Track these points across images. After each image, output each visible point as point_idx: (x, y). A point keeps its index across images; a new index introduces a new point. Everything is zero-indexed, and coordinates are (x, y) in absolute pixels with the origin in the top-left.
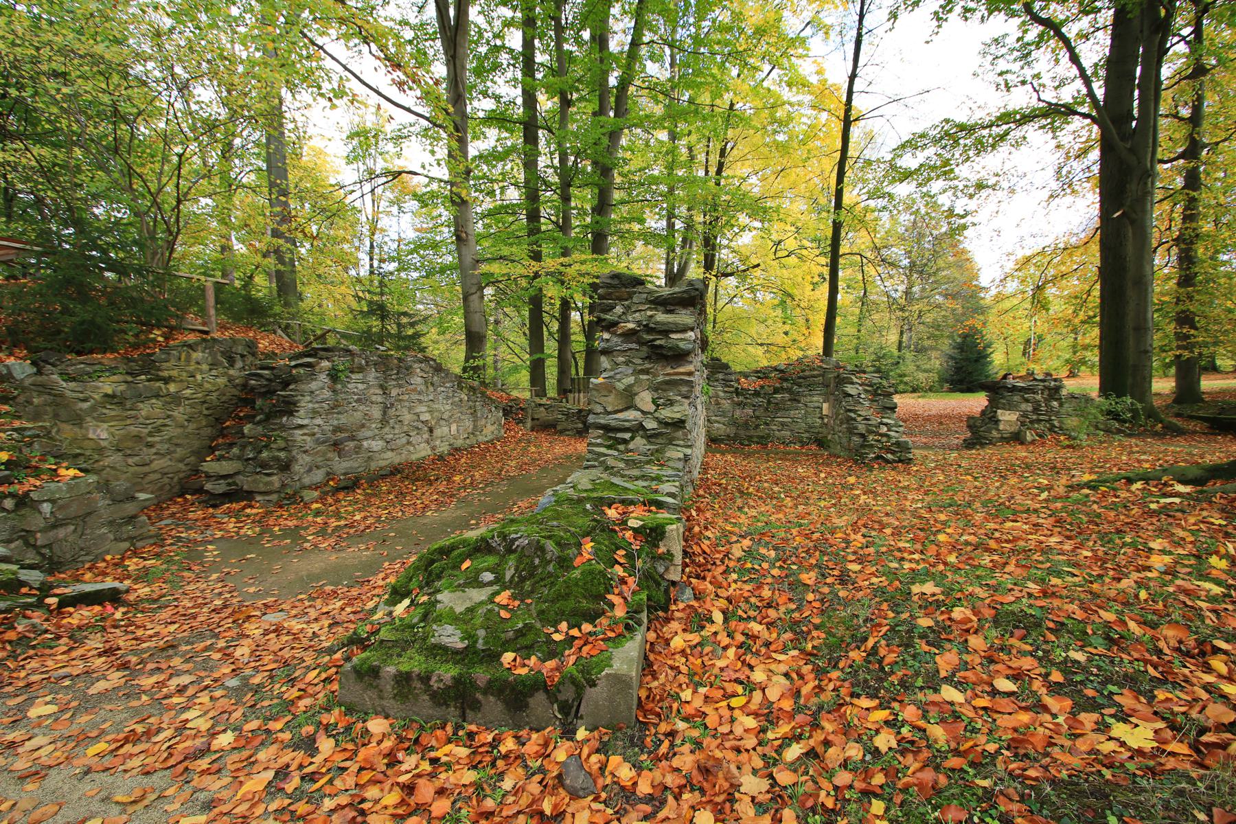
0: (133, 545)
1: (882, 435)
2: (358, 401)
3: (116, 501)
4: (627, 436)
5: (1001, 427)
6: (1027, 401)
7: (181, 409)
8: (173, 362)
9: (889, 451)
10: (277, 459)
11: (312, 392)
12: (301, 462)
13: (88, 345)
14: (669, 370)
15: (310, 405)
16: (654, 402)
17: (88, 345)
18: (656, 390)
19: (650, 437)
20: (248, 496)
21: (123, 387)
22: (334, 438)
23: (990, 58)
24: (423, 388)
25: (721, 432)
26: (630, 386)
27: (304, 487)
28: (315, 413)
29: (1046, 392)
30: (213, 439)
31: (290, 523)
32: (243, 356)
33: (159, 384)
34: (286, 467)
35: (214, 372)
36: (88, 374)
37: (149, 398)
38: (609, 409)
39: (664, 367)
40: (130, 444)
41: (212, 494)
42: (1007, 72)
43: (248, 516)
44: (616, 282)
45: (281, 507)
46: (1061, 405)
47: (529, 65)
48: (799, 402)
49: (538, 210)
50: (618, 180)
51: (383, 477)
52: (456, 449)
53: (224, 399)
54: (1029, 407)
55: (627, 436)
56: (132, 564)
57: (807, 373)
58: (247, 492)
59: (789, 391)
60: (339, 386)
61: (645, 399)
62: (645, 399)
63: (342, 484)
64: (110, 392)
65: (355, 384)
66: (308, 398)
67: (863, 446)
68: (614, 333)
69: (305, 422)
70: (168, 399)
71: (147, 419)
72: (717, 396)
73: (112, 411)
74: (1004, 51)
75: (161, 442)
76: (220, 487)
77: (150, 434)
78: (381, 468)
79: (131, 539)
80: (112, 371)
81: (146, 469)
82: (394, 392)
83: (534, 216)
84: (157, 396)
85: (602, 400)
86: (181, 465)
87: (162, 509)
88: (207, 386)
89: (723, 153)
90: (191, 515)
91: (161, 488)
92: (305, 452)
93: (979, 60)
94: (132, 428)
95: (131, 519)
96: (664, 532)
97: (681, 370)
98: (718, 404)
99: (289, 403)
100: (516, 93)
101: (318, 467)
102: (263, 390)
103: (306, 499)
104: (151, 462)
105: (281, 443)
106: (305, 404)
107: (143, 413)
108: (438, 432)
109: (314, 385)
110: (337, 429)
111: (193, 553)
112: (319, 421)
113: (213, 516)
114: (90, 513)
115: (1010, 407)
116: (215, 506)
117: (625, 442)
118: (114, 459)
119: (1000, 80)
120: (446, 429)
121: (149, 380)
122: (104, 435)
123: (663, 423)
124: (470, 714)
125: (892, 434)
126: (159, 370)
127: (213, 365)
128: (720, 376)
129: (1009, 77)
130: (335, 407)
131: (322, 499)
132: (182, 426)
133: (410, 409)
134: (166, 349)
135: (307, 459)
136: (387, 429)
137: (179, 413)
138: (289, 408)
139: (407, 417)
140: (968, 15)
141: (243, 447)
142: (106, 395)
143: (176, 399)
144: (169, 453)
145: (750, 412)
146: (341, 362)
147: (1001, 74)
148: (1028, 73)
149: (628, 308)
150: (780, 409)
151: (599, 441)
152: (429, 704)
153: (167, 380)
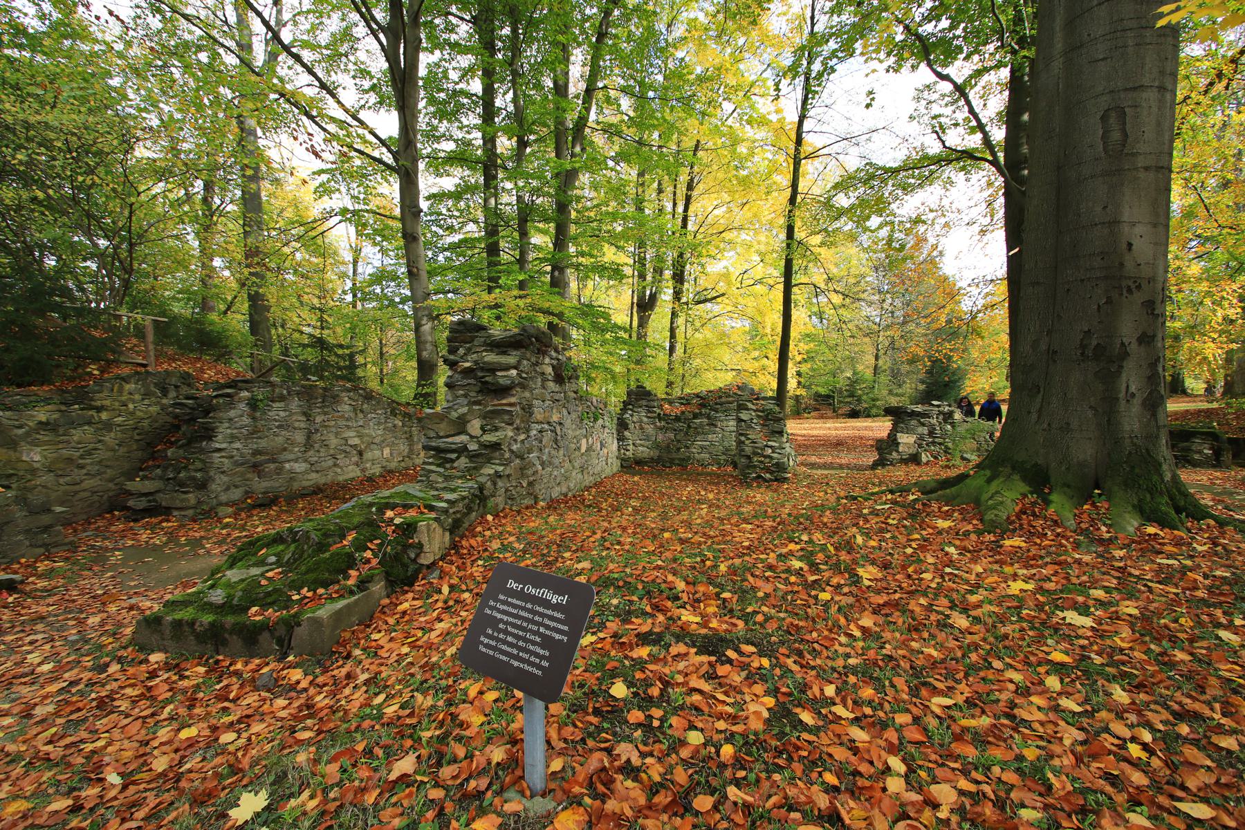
0: (48, 550)
1: (765, 457)
2: (278, 427)
3: (31, 513)
4: (454, 456)
5: (901, 449)
6: (923, 425)
7: (112, 435)
8: (106, 393)
9: (768, 470)
10: (194, 478)
11: (231, 419)
12: (218, 481)
13: (27, 379)
14: (496, 402)
15: (229, 431)
16: (482, 428)
17: (27, 379)
18: (484, 418)
19: (473, 456)
20: (166, 512)
22: (253, 460)
23: (924, 103)
24: (352, 415)
25: (645, 455)
26: (464, 415)
27: (221, 504)
28: (233, 439)
29: (941, 417)
30: (143, 461)
31: (197, 535)
32: (176, 387)
33: (93, 413)
34: (202, 486)
35: (146, 402)
36: (24, 404)
37: (81, 425)
38: (441, 434)
39: (492, 400)
40: (62, 465)
41: (135, 511)
42: (940, 116)
43: (163, 529)
44: (462, 328)
45: (195, 521)
47: (489, 113)
48: (716, 426)
49: (497, 243)
50: (573, 214)
51: (303, 496)
52: (390, 472)
53: (156, 425)
54: (925, 430)
56: (42, 567)
57: (723, 400)
59: (709, 417)
60: (258, 414)
61: (475, 426)
62: (475, 426)
63: (259, 502)
64: (44, 419)
65: (277, 411)
66: (227, 425)
67: (748, 467)
69: (223, 446)
70: (99, 426)
71: (79, 443)
72: (641, 421)
73: (44, 436)
74: (935, 96)
75: (91, 464)
76: (141, 504)
77: (82, 457)
78: (304, 488)
79: (45, 545)
80: (47, 401)
81: (77, 488)
82: (319, 419)
83: (493, 250)
84: (89, 423)
85: (435, 427)
86: (111, 485)
87: (90, 523)
88: (139, 414)
89: (690, 187)
90: (113, 528)
91: (91, 505)
92: (223, 472)
93: (914, 105)
94: (64, 451)
95: (46, 529)
96: (416, 528)
97: (504, 401)
98: (642, 428)
99: (207, 429)
100: (477, 137)
101: (236, 487)
103: (220, 514)
104: (82, 481)
105: (198, 465)
106: (223, 430)
107: (75, 438)
108: (368, 455)
109: (232, 413)
110: (256, 452)
111: (100, 558)
112: (237, 445)
113: (131, 529)
114: (7, 523)
115: (908, 431)
116: (135, 521)
117: (452, 461)
118: (46, 478)
120: (377, 453)
121: (82, 409)
122: (37, 458)
123: (483, 446)
124: (221, 649)
125: (775, 455)
127: (147, 395)
128: (644, 402)
130: (254, 432)
131: (235, 515)
132: (113, 450)
133: (337, 434)
134: (100, 381)
135: (225, 479)
136: (311, 453)
137: (110, 438)
138: (208, 434)
139: (334, 442)
141: (165, 469)
142: (41, 423)
143: (108, 426)
144: (99, 473)
145: (672, 436)
146: (260, 393)
149: (469, 350)
150: (698, 433)
152: (194, 642)
153: (99, 409)
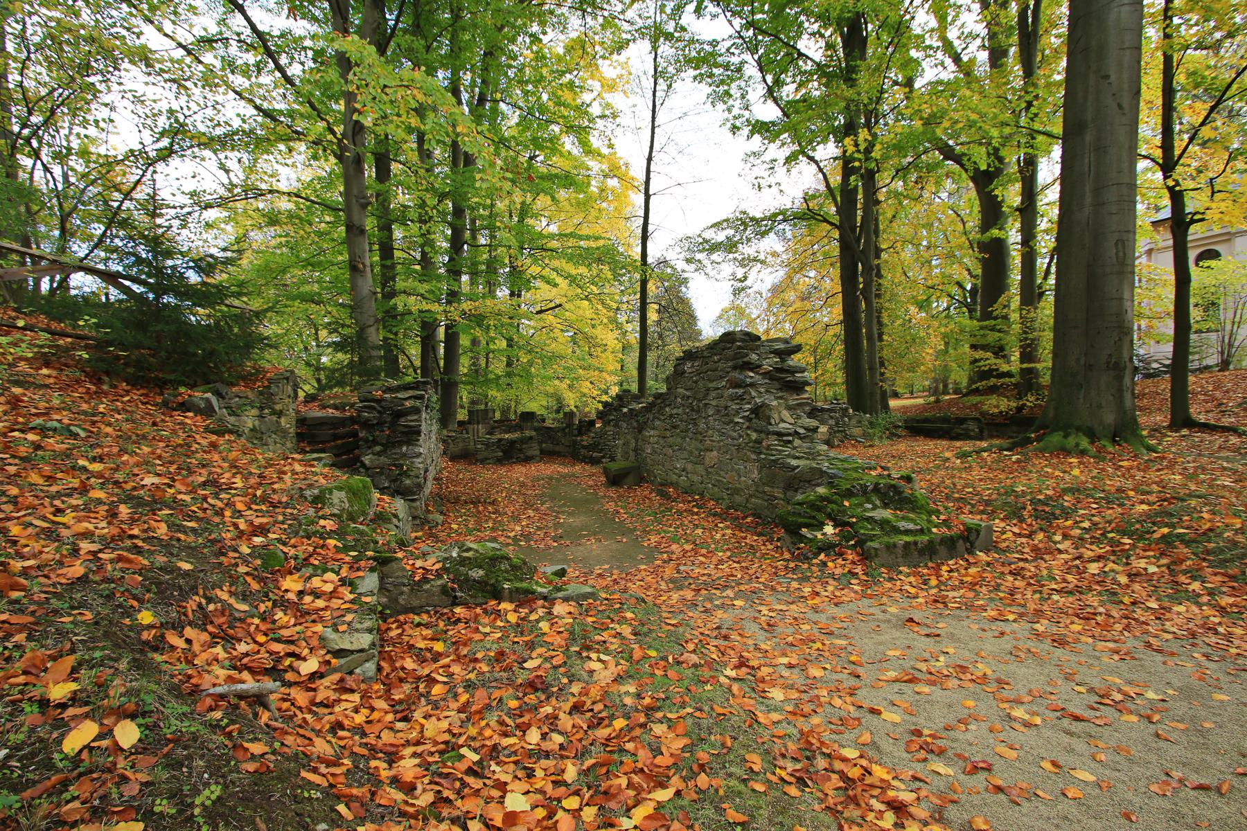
68: (757, 373)
117: (790, 442)
119: (755, 182)
148: (772, 180)
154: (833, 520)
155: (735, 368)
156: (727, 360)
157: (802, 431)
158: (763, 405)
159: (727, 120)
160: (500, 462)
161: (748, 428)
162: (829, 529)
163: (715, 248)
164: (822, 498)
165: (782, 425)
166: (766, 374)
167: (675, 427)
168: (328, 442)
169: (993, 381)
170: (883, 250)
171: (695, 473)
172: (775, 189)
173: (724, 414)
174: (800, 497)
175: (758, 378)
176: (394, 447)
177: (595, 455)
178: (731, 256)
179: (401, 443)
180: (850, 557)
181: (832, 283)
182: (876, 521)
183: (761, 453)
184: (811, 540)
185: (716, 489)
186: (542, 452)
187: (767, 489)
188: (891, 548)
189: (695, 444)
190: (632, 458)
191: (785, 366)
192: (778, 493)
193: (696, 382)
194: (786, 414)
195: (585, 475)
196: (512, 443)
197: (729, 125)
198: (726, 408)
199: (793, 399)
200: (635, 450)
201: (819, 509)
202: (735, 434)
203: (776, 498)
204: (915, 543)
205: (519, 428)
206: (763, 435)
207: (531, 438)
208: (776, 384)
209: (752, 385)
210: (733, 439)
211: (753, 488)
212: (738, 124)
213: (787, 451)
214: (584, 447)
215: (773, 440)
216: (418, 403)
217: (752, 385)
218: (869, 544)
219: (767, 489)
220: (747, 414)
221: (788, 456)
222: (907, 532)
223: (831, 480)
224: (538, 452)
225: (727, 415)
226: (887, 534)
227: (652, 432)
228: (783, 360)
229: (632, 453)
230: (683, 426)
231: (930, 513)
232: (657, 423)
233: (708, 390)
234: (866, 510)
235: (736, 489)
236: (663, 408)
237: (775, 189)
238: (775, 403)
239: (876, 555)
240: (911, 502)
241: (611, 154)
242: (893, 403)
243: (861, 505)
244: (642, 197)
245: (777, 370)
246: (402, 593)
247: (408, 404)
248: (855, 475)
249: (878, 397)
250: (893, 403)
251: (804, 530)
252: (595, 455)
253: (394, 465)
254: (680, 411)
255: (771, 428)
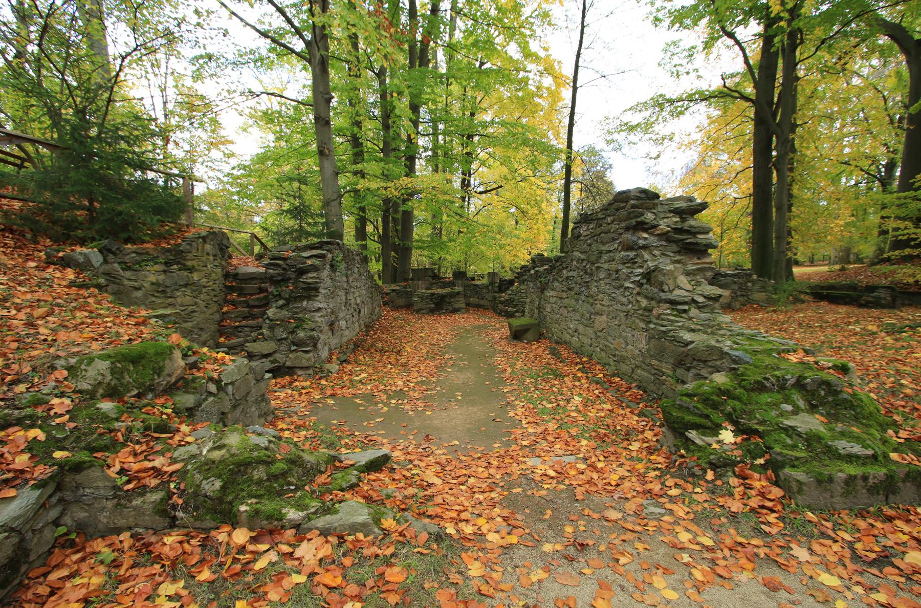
4: (686, 307)
21: (162, 277)
23: (669, 54)
36: (139, 263)
39: (691, 258)
44: (643, 196)
46: (753, 285)
55: (686, 307)
58: (288, 368)
64: (154, 281)
68: (652, 234)
93: (662, 55)
102: (280, 278)
117: (685, 311)
119: (674, 70)
126: (186, 260)
129: (679, 68)
140: (658, 23)
147: (675, 66)
148: (690, 67)
151: (668, 311)
153: (191, 270)
154: (735, 423)
155: (627, 229)
156: (621, 221)
157: (701, 299)
158: (656, 269)
159: (651, 13)
160: (432, 312)
161: (638, 294)
162: (727, 436)
163: (632, 129)
164: (721, 392)
165: (678, 292)
166: (661, 236)
167: (570, 289)
168: (255, 294)
169: (907, 251)
170: (797, 126)
171: (585, 335)
172: (693, 75)
173: (615, 277)
174: (690, 386)
175: (652, 240)
176: (295, 301)
177: (510, 309)
178: (647, 136)
179: (302, 298)
180: (757, 484)
181: (744, 160)
182: (799, 435)
183: (650, 322)
184: (700, 448)
185: (603, 354)
186: (468, 305)
187: (654, 362)
188: (825, 482)
189: (587, 306)
190: (536, 315)
191: (686, 226)
192: (667, 368)
193: (590, 245)
194: (683, 280)
195: (500, 328)
196: (443, 297)
197: (652, 18)
198: (617, 271)
199: (692, 264)
200: (539, 308)
201: (715, 406)
202: (624, 300)
203: (664, 373)
204: (865, 478)
205: (451, 284)
206: (654, 303)
207: (458, 293)
208: (674, 247)
209: (645, 247)
210: (622, 304)
211: (640, 359)
212: (660, 16)
213: (681, 322)
214: (502, 303)
215: (665, 309)
216: (317, 262)
217: (645, 247)
218: (788, 470)
219: (654, 362)
220: (637, 279)
221: (681, 327)
222: (850, 458)
223: (734, 367)
224: (463, 306)
225: (617, 279)
226: (816, 457)
227: (552, 293)
228: (683, 220)
229: (536, 311)
230: (576, 289)
231: (883, 427)
232: (556, 284)
233: (601, 252)
234: (782, 414)
235: (622, 356)
236: (561, 271)
237: (693, 75)
238: (670, 267)
239: (800, 491)
240: (852, 407)
241: (547, 56)
242: (796, 270)
243: (776, 405)
244: (571, 90)
245: (677, 231)
246: (103, 509)
247: (309, 262)
248: (768, 361)
249: (784, 264)
250: (796, 270)
251: (692, 434)
252: (510, 309)
253: (293, 318)
254: (575, 274)
255: (663, 296)
